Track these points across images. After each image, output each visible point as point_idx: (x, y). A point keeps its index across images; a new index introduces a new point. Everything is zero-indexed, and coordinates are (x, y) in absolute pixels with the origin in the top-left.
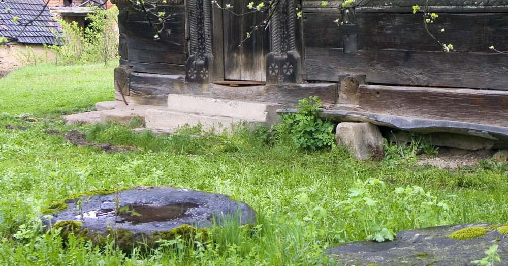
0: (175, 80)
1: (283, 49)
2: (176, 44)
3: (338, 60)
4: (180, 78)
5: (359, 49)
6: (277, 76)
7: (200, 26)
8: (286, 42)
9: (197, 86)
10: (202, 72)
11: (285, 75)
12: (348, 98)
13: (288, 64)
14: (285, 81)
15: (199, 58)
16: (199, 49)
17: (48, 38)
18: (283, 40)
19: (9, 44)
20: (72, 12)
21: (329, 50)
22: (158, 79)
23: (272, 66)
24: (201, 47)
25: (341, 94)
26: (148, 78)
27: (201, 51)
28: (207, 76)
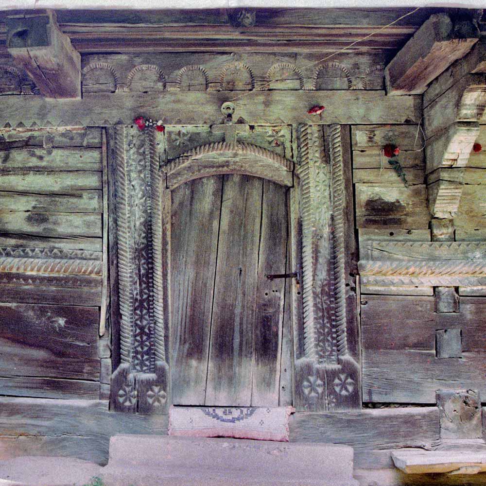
0: (84, 408)
1: (321, 353)
2: (78, 343)
3: (428, 369)
4: (97, 405)
5: (463, 352)
6: (321, 397)
7: (138, 312)
8: (328, 341)
9: (136, 419)
10: (121, 392)
11: (338, 396)
12: (458, 428)
13: (343, 377)
14: (339, 404)
15: (135, 368)
16: (137, 352)
17: (336, 175)
18: (322, 337)
19: (104, 148)
20: (406, 46)
21: (410, 354)
22: (42, 409)
23: (340, 380)
24: (139, 349)
25: (446, 423)
26: (20, 405)
27: (139, 356)
28: (163, 401)
